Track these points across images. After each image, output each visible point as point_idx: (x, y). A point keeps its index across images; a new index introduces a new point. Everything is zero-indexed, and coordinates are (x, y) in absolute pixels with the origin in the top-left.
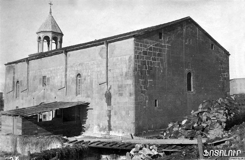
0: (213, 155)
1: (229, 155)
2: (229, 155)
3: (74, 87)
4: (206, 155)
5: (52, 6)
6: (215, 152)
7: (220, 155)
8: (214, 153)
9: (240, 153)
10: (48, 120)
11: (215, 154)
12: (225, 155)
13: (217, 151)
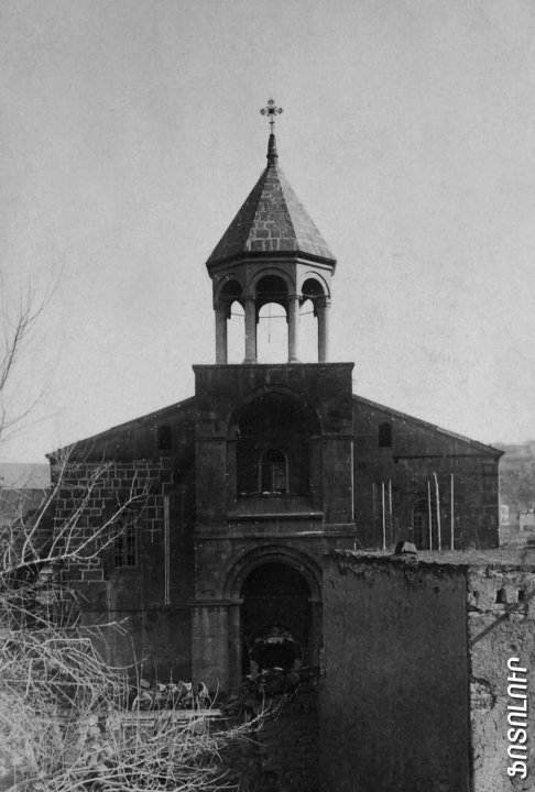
0: (525, 748)
1: (525, 697)
2: (525, 697)
3: (222, 585)
4: (524, 770)
5: (277, 118)
6: (514, 740)
7: (524, 724)
8: (516, 743)
9: (517, 660)
10: (264, 250)
11: (522, 741)
12: (525, 709)
13: (513, 734)
